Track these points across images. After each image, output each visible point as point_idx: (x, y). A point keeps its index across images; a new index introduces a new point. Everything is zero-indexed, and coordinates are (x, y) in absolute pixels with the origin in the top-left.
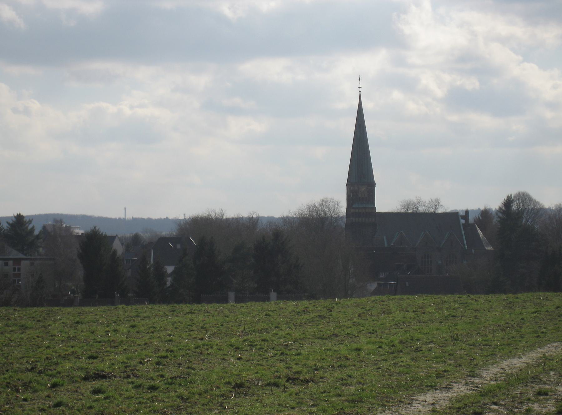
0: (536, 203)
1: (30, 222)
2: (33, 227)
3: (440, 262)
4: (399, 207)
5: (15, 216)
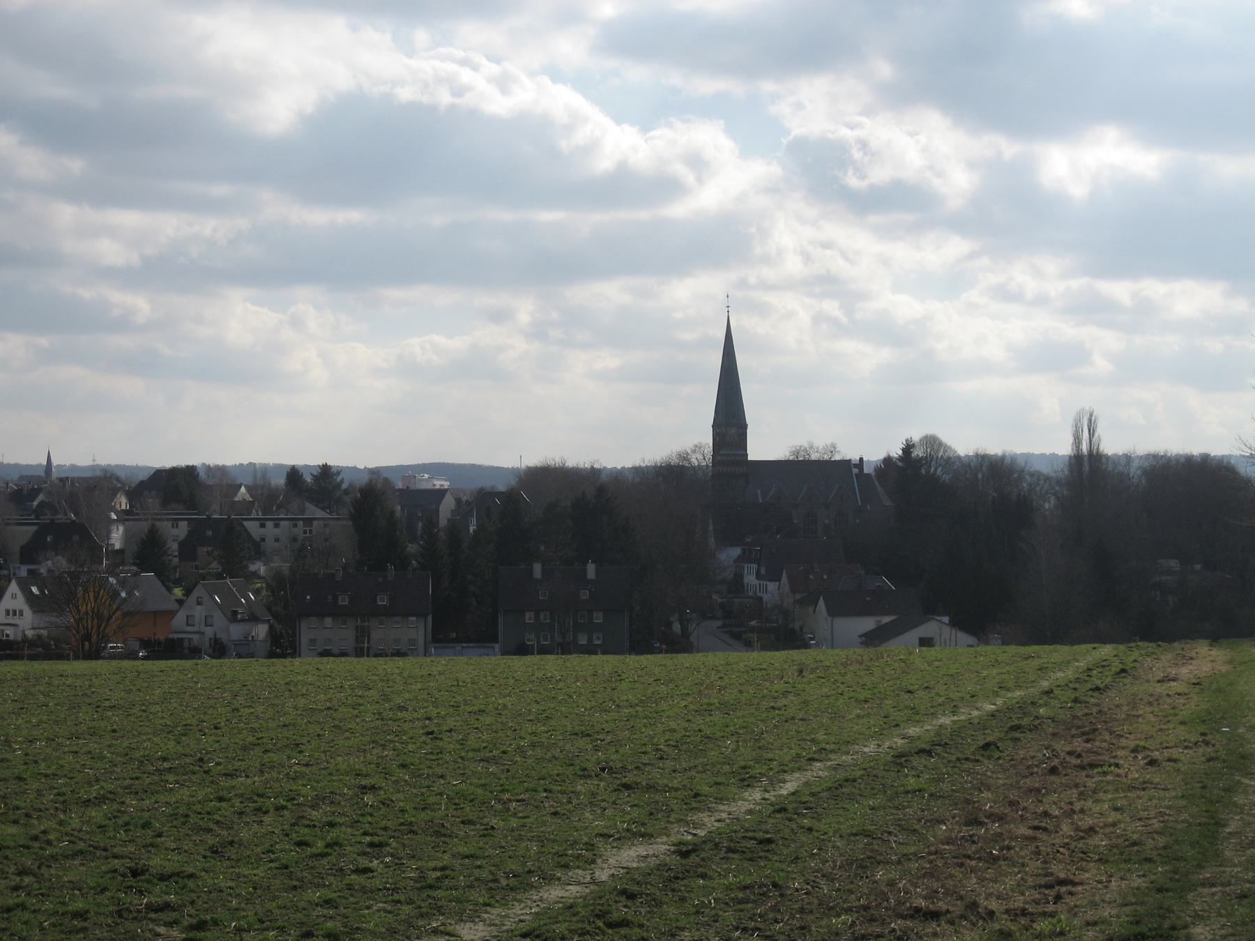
0: (947, 448)
1: (338, 473)
2: (343, 479)
3: (827, 521)
4: (788, 454)
5: (319, 466)
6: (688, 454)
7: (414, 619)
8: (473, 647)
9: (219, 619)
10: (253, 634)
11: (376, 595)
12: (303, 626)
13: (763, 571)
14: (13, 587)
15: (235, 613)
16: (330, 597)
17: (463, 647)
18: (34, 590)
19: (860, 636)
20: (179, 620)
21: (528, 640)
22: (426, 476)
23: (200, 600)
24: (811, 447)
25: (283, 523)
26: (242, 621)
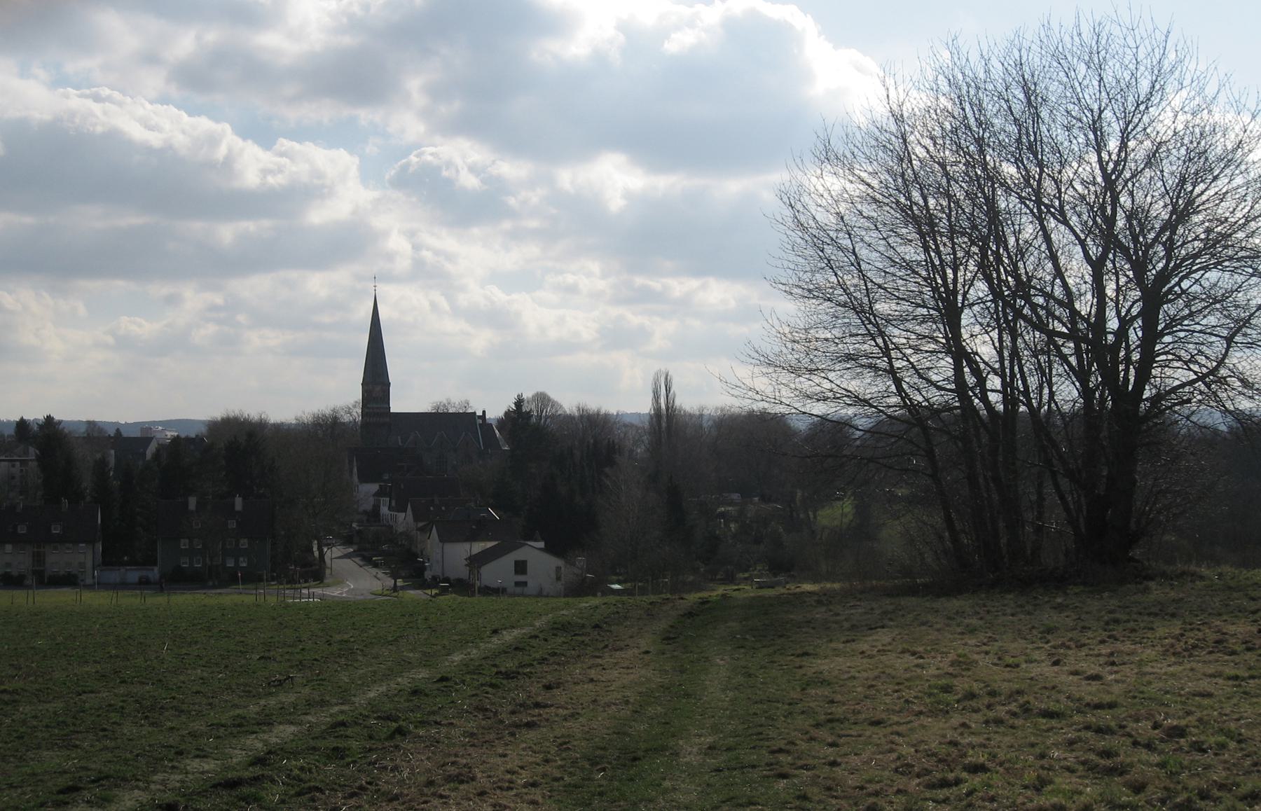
0: (554, 404)
3: (455, 463)
6: (350, 408)
13: (393, 504)
19: (466, 559)
21: (183, 563)
22: (160, 428)
24: (449, 403)
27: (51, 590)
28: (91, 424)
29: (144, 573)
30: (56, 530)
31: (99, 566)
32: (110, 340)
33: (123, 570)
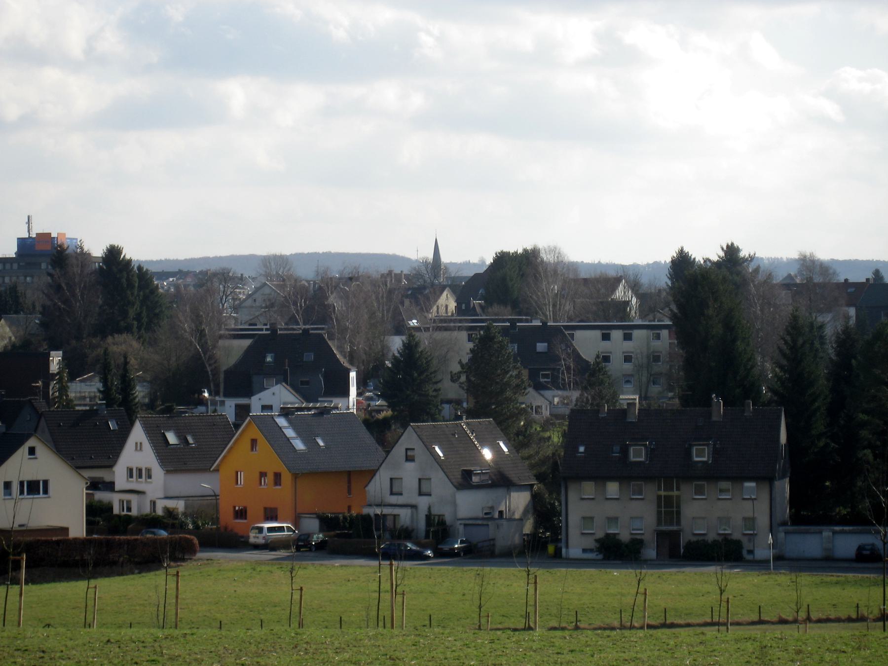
7: (753, 484)
8: (850, 532)
9: (440, 485)
10: (502, 508)
11: (691, 446)
12: (573, 496)
14: (138, 433)
15: (467, 474)
16: (616, 448)
17: (834, 533)
18: (172, 438)
20: (378, 486)
23: (409, 453)
25: (636, 333)
26: (479, 487)
27: (688, 570)
28: (808, 264)
29: (867, 539)
30: (701, 455)
31: (784, 524)
32: (831, 109)
33: (827, 533)
